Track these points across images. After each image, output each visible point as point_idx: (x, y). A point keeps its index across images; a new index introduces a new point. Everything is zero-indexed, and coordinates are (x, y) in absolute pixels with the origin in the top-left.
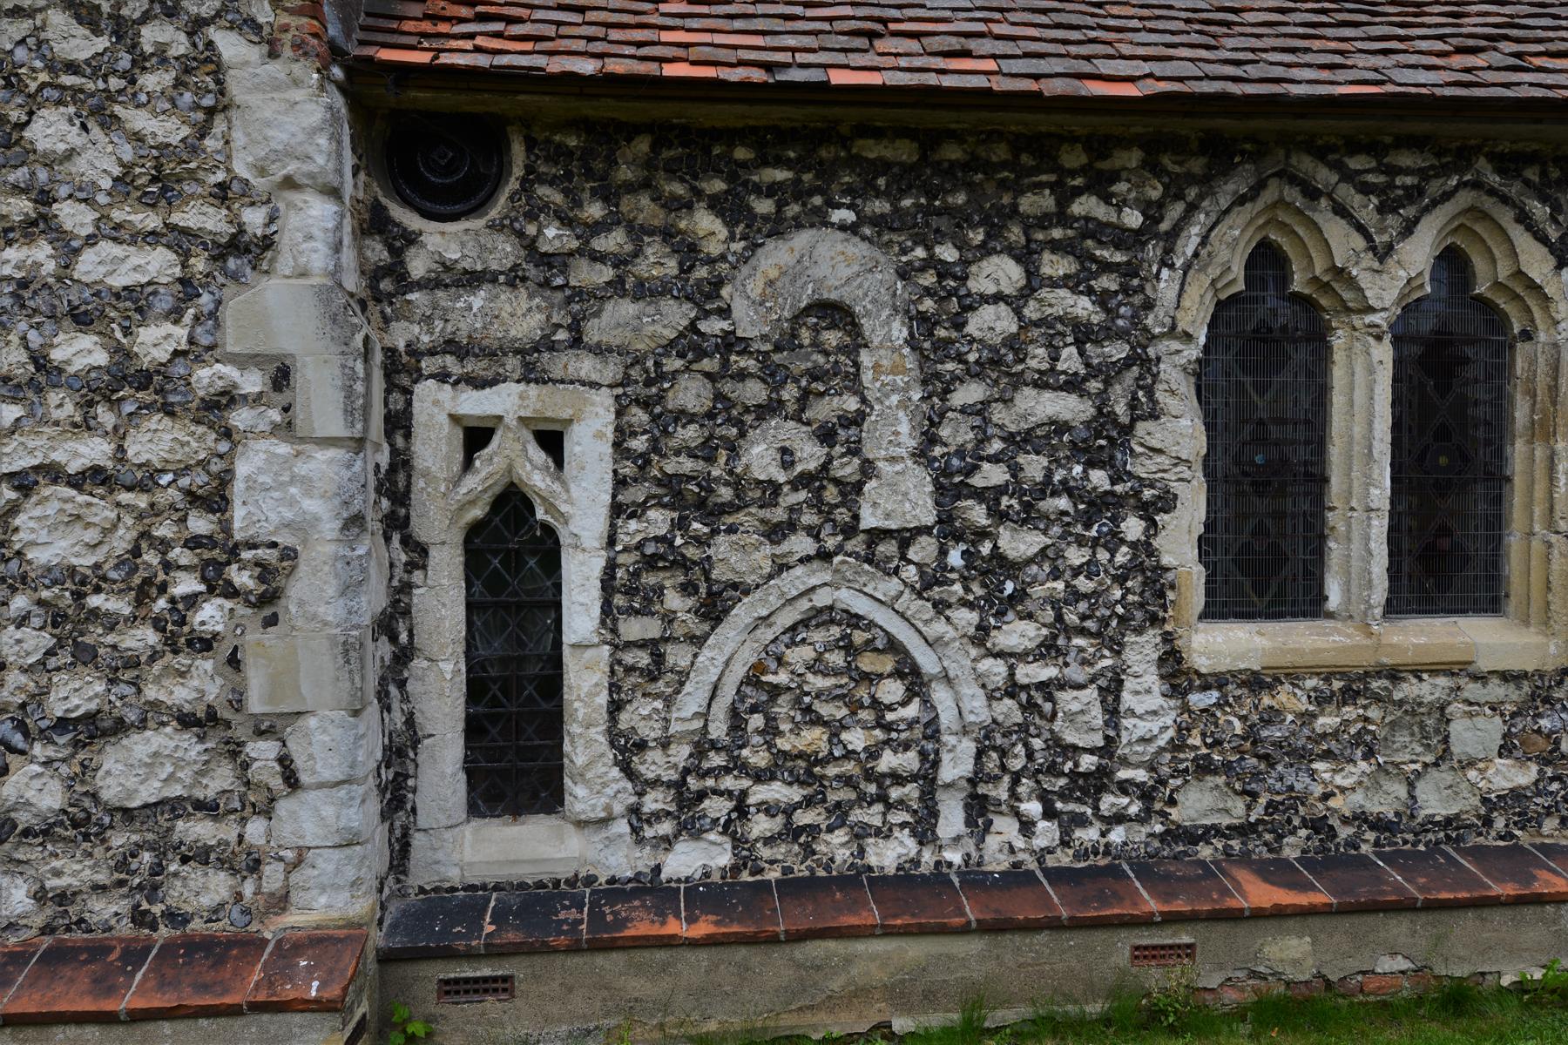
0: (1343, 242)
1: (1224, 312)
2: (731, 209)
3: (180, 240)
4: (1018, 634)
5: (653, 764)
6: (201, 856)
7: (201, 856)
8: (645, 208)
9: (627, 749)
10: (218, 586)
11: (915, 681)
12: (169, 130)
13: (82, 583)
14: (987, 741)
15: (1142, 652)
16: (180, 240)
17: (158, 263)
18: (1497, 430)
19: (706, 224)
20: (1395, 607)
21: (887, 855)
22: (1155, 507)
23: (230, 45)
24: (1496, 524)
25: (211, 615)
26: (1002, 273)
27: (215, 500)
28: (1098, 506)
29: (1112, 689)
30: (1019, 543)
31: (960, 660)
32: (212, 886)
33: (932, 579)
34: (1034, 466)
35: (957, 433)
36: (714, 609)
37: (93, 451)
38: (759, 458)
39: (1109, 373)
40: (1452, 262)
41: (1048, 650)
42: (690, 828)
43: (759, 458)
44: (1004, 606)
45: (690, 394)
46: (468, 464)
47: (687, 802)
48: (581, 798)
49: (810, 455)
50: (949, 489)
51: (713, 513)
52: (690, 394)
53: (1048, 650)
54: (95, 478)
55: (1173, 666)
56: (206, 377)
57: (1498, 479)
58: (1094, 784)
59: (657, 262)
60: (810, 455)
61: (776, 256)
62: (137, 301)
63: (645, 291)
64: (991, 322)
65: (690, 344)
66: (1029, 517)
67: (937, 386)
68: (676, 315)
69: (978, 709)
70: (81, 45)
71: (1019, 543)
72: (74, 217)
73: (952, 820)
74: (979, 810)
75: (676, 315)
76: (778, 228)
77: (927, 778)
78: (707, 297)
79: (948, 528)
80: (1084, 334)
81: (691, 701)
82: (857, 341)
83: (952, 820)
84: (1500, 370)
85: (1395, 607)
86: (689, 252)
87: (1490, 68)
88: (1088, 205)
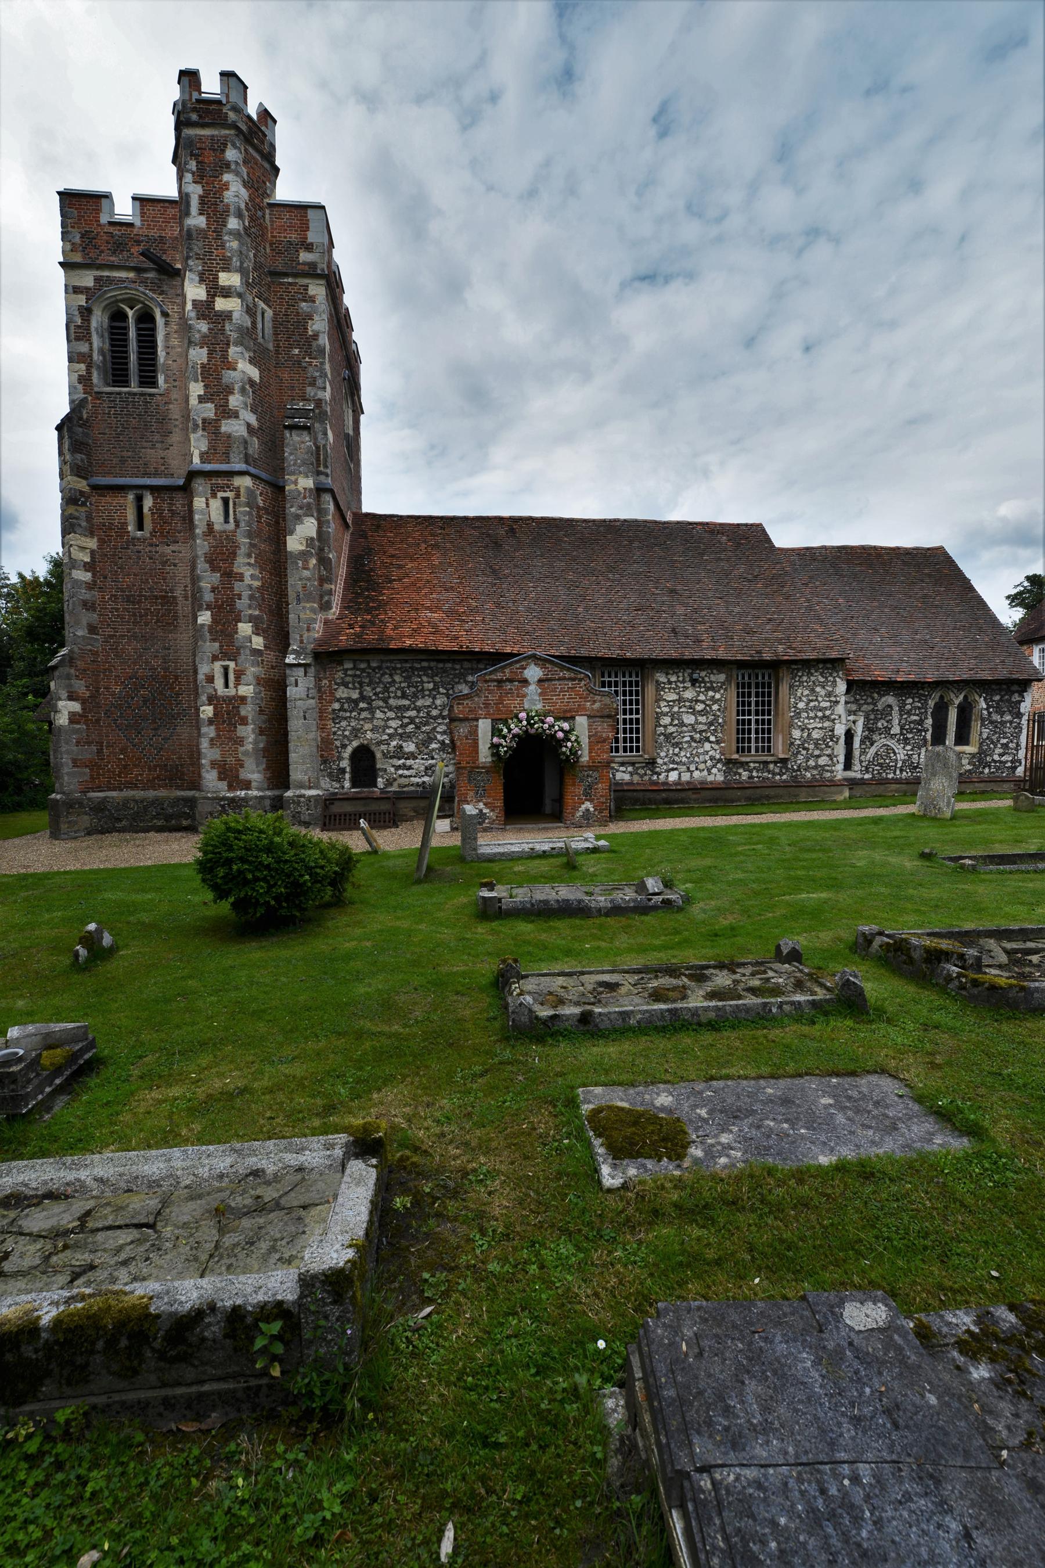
0: (952, 696)
1: (936, 704)
2: (878, 693)
3: (830, 701)
4: (908, 747)
5: (864, 764)
6: (827, 771)
7: (827, 771)
8: (868, 693)
9: (861, 762)
10: (832, 740)
11: (895, 754)
12: (830, 689)
13: (818, 740)
14: (904, 761)
15: (923, 750)
16: (830, 701)
17: (828, 704)
18: (970, 720)
19: (876, 695)
20: (955, 745)
21: (890, 776)
22: (926, 731)
23: (838, 679)
24: (969, 733)
25: (831, 744)
26: (910, 701)
27: (833, 731)
28: (920, 731)
29: (919, 755)
30: (910, 736)
31: (901, 751)
32: (829, 774)
33: (899, 740)
34: (912, 725)
35: (903, 722)
36: (872, 745)
37: (820, 725)
38: (879, 725)
39: (922, 713)
40: (966, 697)
41: (912, 750)
42: (867, 772)
43: (879, 725)
44: (906, 744)
45: (872, 717)
46: (512, 655)
47: (867, 768)
48: (856, 768)
49: (886, 724)
50: (902, 729)
51: (873, 732)
52: (872, 717)
53: (912, 750)
54: (820, 728)
55: (927, 750)
56: (833, 717)
57: (969, 727)
58: (917, 767)
59: (870, 700)
60: (886, 724)
61: (883, 699)
62: (826, 709)
63: (868, 704)
64: (908, 707)
65: (873, 710)
66: (911, 732)
67: (901, 715)
68: (872, 707)
69: (903, 757)
70: (822, 680)
71: (910, 736)
72: (820, 699)
73: (898, 772)
74: (901, 771)
75: (872, 707)
76: (884, 695)
77: (896, 766)
78: (875, 704)
79: (901, 734)
80: (919, 708)
81: (869, 756)
82: (892, 709)
83: (898, 772)
84: (971, 711)
85: (955, 745)
86: (873, 698)
87: (929, 935)
88: (921, 692)
